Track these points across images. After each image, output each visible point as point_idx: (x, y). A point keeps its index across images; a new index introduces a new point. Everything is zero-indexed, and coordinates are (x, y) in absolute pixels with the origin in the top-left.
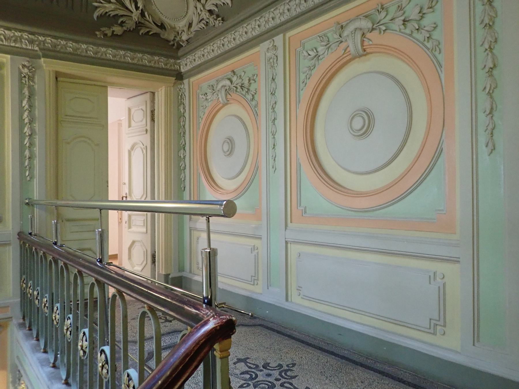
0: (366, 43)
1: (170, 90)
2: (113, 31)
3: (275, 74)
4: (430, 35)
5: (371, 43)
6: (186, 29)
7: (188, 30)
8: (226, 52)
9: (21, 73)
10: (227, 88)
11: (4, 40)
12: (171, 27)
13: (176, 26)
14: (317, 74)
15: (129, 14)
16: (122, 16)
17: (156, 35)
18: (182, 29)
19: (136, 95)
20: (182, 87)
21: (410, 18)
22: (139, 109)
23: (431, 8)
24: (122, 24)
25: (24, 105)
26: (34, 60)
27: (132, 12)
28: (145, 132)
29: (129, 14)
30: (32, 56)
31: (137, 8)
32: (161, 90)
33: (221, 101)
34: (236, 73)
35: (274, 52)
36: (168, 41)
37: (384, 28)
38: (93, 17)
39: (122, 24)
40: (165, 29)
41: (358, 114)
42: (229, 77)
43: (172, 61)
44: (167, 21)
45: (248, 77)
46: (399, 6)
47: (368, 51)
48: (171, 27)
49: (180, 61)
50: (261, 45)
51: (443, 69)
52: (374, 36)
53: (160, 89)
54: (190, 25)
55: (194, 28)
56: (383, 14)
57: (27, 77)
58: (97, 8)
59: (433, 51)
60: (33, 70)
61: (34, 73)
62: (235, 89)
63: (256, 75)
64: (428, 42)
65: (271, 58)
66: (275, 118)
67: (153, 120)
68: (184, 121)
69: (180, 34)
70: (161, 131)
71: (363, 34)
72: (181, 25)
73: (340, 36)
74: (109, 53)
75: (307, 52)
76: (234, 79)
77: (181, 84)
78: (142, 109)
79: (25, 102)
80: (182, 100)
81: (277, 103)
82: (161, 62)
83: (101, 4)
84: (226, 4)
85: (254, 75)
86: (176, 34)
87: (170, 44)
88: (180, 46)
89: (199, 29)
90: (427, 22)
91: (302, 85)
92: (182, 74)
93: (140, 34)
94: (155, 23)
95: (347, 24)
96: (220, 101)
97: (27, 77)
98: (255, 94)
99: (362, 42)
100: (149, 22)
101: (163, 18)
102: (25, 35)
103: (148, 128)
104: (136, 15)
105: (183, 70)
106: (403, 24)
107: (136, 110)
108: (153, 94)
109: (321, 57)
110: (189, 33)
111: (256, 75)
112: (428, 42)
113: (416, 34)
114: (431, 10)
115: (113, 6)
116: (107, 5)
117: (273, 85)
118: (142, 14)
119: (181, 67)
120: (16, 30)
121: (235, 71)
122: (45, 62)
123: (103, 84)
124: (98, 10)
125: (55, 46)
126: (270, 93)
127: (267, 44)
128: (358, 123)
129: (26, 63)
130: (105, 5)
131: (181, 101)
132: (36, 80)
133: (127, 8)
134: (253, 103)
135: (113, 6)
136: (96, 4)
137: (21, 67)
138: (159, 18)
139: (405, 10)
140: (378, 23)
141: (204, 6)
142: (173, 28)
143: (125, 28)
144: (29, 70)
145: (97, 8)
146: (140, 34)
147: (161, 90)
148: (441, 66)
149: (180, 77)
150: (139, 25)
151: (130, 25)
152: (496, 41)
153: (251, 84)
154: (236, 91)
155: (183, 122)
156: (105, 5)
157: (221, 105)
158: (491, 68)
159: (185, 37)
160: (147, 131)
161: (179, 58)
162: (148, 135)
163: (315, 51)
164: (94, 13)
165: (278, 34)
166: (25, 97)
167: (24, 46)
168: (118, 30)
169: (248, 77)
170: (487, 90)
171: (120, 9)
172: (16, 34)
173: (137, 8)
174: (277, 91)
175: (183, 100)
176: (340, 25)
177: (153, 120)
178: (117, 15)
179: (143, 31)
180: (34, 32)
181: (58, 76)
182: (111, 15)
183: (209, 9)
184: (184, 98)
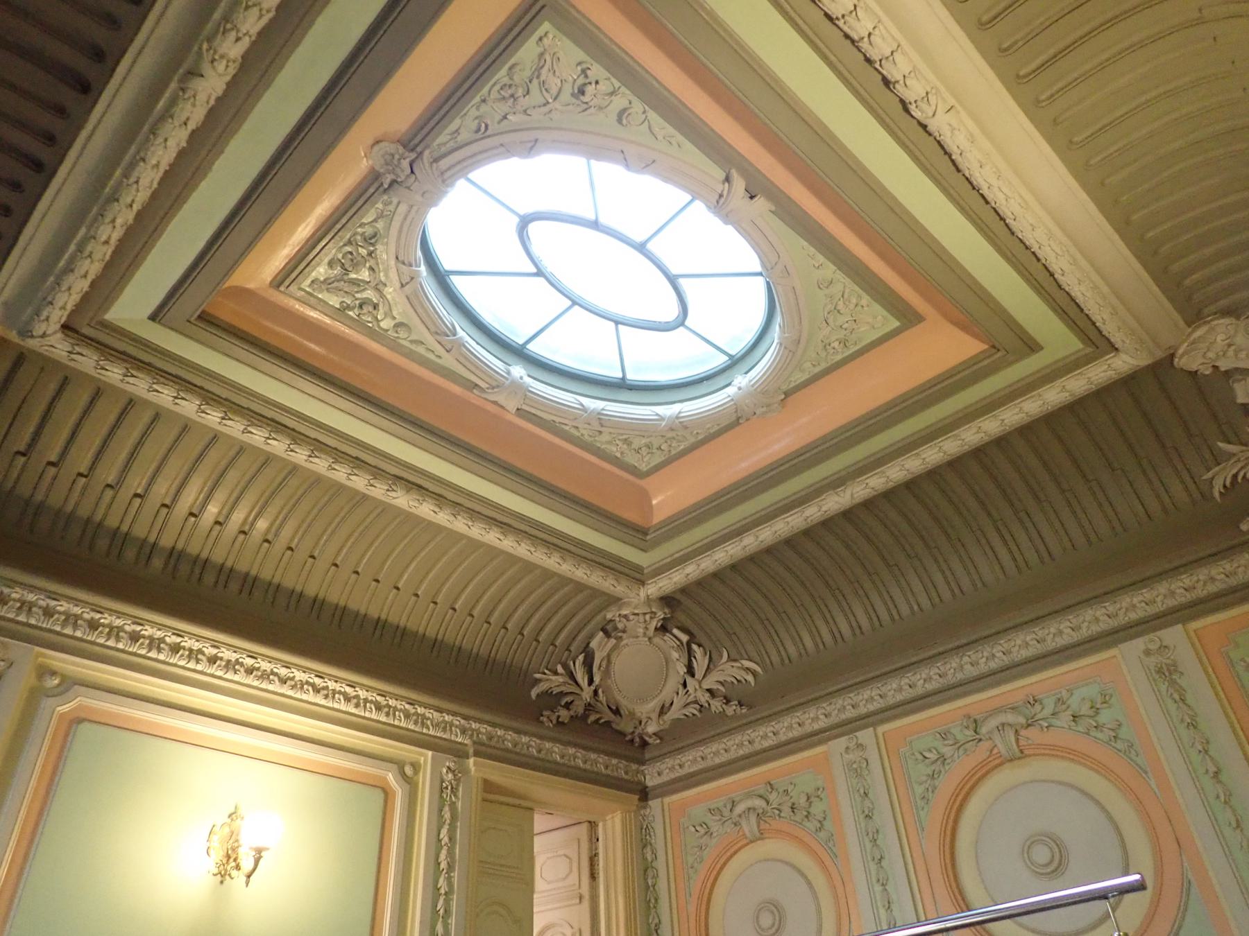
0: (1022, 742)
1: (630, 817)
2: (559, 717)
3: (867, 787)
4: (1117, 735)
5: (1030, 742)
6: (654, 716)
7: (659, 716)
8: (757, 753)
9: (442, 781)
10: (761, 811)
11: (431, 728)
12: (629, 712)
13: (636, 711)
14: (947, 785)
15: (577, 691)
16: (567, 694)
17: (608, 723)
18: (648, 715)
19: (568, 824)
20: (647, 813)
21: (1081, 713)
22: (560, 856)
23: (1105, 703)
24: (568, 706)
25: (441, 836)
26: (461, 760)
27: (582, 689)
28: (578, 901)
29: (577, 691)
30: (459, 753)
31: (591, 681)
32: (613, 818)
33: (748, 834)
34: (775, 787)
35: (861, 754)
36: (623, 734)
37: (1046, 725)
38: (530, 695)
39: (568, 706)
40: (621, 716)
41: (763, 908)
42: (762, 792)
43: (634, 767)
44: (625, 704)
45: (803, 792)
46: (1059, 699)
47: (1026, 752)
48: (629, 712)
49: (644, 767)
50: (830, 743)
51: (1150, 774)
52: (1033, 734)
53: (610, 816)
54: (663, 711)
55: (674, 714)
56: (1038, 707)
57: (449, 788)
58: (539, 681)
59: (1127, 753)
60: (459, 773)
61: (458, 780)
62: (777, 812)
63: (821, 789)
64: (1116, 742)
65: (855, 762)
66: (881, 857)
67: (593, 876)
68: (656, 877)
69: (643, 724)
70: (616, 897)
71: (1016, 731)
72: (646, 709)
73: (975, 732)
74: (555, 751)
75: (921, 754)
76: (773, 797)
77: (645, 808)
78: (566, 856)
79: (444, 832)
80: (648, 837)
81: (880, 832)
82: (618, 768)
83: (544, 676)
84: (744, 681)
85: (818, 789)
86: (637, 723)
87: (627, 739)
88: (644, 744)
89: (683, 717)
90: (1105, 717)
91: (920, 803)
92: (647, 790)
93: (589, 722)
94: (608, 706)
95: (986, 718)
96: (744, 834)
97: (449, 788)
98: (825, 818)
99: (1017, 740)
100: (602, 704)
101: (619, 697)
102: (457, 721)
103: (585, 889)
104: (587, 694)
105: (649, 783)
106: (1074, 721)
107: (548, 858)
108: (593, 825)
109: (947, 761)
110: (661, 722)
111: (821, 789)
112: (1116, 742)
113: (1094, 733)
114: (1105, 705)
115: (561, 679)
116: (554, 678)
117: (867, 803)
118: (596, 692)
119: (647, 777)
120: (449, 712)
121: (772, 782)
122: (475, 764)
123: (528, 804)
124: (542, 684)
125: (490, 738)
126: (862, 817)
127: (842, 742)
128: (1042, 854)
129: (452, 765)
130: (551, 677)
131: (646, 840)
132: (460, 794)
133: (576, 683)
134: (822, 834)
135: (561, 679)
136: (538, 676)
137: (445, 770)
138: (615, 700)
139: (1069, 702)
140: (1032, 718)
141: (700, 682)
142: (632, 714)
143: (572, 713)
144: (455, 775)
145: (539, 681)
146: (589, 722)
147: (613, 818)
148: (1146, 773)
149: (644, 794)
150: (589, 707)
151: (579, 708)
152: (1208, 742)
153: (811, 803)
154: (779, 815)
155: (652, 878)
156: (551, 677)
157: (745, 842)
158: (1216, 773)
159: (651, 729)
160: (581, 898)
161: (642, 763)
162: (586, 904)
163: (934, 751)
164: (530, 691)
165: (866, 727)
166: (444, 823)
167: (453, 738)
168: (564, 714)
169: (803, 792)
170: (1222, 799)
171: (569, 684)
172: (447, 718)
173: (591, 681)
174: (875, 812)
175: (650, 836)
176: (972, 719)
177: (593, 876)
178: (562, 692)
179: (592, 718)
180: (469, 716)
181: (488, 787)
182: (554, 693)
183: (708, 687)
184: (652, 834)
